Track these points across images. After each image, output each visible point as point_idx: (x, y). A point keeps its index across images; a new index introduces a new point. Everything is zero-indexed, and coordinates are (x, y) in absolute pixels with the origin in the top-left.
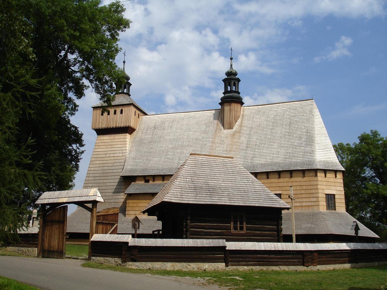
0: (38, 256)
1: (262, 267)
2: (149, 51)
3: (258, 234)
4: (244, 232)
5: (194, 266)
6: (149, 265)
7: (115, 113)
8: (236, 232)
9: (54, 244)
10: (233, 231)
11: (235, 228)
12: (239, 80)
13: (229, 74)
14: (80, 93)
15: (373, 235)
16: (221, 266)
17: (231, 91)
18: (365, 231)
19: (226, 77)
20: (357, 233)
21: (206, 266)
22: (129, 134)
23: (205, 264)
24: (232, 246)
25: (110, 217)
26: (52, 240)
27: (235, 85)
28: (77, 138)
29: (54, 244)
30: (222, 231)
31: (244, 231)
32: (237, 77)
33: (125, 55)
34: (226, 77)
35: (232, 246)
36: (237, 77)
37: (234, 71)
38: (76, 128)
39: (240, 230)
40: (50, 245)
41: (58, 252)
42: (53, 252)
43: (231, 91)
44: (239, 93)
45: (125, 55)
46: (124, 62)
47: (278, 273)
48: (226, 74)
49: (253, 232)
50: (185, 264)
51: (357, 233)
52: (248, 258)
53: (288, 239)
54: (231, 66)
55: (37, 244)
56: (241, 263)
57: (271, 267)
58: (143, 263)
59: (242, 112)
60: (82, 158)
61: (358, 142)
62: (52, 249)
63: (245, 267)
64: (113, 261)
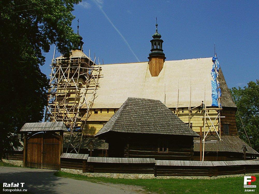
1: (179, 177)
3: (177, 153)
5: (132, 176)
6: (101, 175)
8: (161, 152)
9: (35, 158)
10: (159, 152)
11: (161, 150)
12: (162, 41)
14: (47, 49)
16: (152, 176)
17: (157, 49)
19: (153, 39)
21: (141, 176)
22: (70, 101)
23: (140, 174)
24: (159, 163)
27: (159, 45)
28: (45, 82)
29: (35, 158)
30: (152, 151)
32: (161, 39)
33: (78, 21)
34: (153, 39)
35: (159, 163)
36: (161, 39)
38: (45, 76)
39: (164, 151)
43: (157, 49)
44: (162, 51)
45: (78, 21)
46: (78, 27)
47: (179, 181)
49: (173, 152)
50: (126, 175)
52: (170, 171)
53: (196, 156)
56: (166, 174)
57: (236, 175)
58: (217, 165)
59: (165, 65)
61: (247, 86)
63: (168, 177)
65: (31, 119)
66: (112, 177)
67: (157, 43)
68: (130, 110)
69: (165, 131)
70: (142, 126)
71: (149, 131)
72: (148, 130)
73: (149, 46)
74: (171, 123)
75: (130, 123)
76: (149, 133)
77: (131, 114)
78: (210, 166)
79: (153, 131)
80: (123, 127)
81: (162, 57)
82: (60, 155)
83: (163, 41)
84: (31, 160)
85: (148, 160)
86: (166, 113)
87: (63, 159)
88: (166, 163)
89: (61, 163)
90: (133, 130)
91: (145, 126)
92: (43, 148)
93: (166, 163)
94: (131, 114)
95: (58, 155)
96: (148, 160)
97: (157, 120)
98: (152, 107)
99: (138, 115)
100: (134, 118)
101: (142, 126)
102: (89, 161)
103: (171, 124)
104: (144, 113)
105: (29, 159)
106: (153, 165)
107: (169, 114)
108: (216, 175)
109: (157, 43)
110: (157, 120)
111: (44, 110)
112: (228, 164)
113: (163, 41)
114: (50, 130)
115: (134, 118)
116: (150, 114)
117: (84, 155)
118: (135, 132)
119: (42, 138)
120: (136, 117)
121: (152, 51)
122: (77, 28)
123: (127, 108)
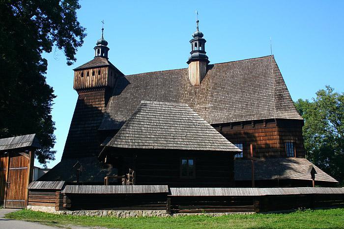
7: (93, 74)
15: (332, 179)
18: (321, 176)
20: (313, 177)
24: (175, 192)
35: (175, 192)
44: (205, 53)
46: (103, 29)
51: (313, 177)
61: (315, 97)
65: (69, 3)
73: (189, 48)
77: (142, 123)
78: (238, 188)
79: (171, 146)
80: (127, 141)
81: (203, 61)
85: (157, 189)
86: (194, 121)
88: (186, 192)
90: (141, 144)
91: (160, 139)
93: (186, 192)
94: (142, 123)
96: (157, 189)
100: (146, 129)
101: (156, 139)
111: (50, 114)
115: (146, 129)
121: (191, 53)
123: (138, 115)
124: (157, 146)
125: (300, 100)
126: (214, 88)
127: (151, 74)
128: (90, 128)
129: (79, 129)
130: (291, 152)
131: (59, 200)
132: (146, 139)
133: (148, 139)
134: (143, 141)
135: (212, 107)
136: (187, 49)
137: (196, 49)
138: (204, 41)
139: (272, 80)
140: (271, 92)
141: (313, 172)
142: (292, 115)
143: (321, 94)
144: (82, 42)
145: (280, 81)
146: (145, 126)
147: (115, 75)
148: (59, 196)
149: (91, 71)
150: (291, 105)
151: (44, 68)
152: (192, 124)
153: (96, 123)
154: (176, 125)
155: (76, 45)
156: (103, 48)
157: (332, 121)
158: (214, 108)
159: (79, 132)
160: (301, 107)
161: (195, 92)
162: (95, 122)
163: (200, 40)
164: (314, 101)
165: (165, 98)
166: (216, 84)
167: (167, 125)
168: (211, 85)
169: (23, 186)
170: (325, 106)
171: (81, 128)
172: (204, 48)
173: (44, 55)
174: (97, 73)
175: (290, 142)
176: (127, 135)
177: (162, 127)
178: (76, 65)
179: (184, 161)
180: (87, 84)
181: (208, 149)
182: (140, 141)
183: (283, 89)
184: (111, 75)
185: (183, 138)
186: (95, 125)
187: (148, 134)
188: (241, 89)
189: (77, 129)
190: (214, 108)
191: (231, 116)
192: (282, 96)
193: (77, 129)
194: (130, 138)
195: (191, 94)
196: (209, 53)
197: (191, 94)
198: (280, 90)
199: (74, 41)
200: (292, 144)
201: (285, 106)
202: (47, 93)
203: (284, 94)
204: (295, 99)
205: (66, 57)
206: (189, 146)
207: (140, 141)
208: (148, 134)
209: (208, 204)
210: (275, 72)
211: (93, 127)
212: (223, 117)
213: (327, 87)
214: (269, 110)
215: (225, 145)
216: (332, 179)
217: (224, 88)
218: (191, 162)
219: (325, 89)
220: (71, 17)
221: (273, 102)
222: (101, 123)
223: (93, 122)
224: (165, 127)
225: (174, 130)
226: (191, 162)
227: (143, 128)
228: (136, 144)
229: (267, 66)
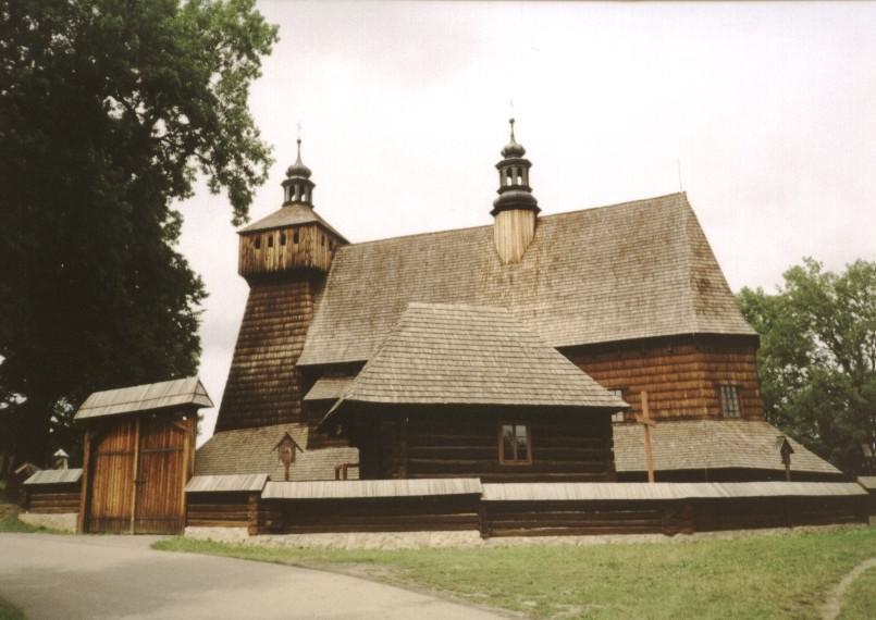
0: (77, 533)
2: (536, 202)
4: (526, 464)
7: (283, 242)
8: (511, 463)
13: (508, 152)
15: (826, 467)
16: (471, 537)
17: (515, 187)
18: (803, 459)
20: (786, 461)
24: (495, 492)
25: (323, 258)
26: (110, 495)
27: (520, 174)
31: (529, 462)
34: (503, 159)
35: (495, 492)
36: (524, 157)
37: (518, 147)
40: (104, 507)
41: (119, 519)
42: (112, 519)
44: (529, 190)
46: (299, 142)
48: (502, 154)
51: (786, 461)
54: (512, 136)
55: (78, 505)
60: (203, 311)
61: (783, 283)
62: (108, 514)
64: (234, 534)
66: (341, 546)
67: (514, 170)
68: (412, 339)
69: (517, 396)
70: (446, 383)
71: (466, 395)
72: (462, 395)
74: (539, 371)
75: (408, 377)
76: (465, 401)
79: (480, 398)
82: (183, 484)
83: (678, 200)
84: (101, 511)
86: (523, 344)
87: (193, 497)
89: (187, 509)
91: (454, 383)
92: (138, 465)
95: (180, 478)
97: (495, 364)
98: (478, 328)
99: (435, 352)
101: (446, 383)
102: (266, 495)
103: (535, 376)
104: (454, 347)
105: (97, 505)
106: (473, 500)
107: (531, 345)
108: (687, 530)
109: (514, 170)
110: (495, 364)
112: (729, 493)
113: (678, 200)
114: (159, 406)
115: (424, 361)
116: (471, 347)
117: (255, 478)
118: (423, 401)
119: (137, 435)
120: (429, 357)
121: (500, 192)
122: (296, 144)
124: (451, 398)
125: (745, 291)
126: (553, 268)
127: (410, 240)
128: (278, 362)
129: (254, 364)
130: (731, 408)
131: (256, 513)
132: (425, 383)
133: (430, 383)
134: (421, 389)
135: (549, 310)
136: (489, 186)
137: (509, 182)
138: (528, 164)
139: (683, 248)
140: (683, 274)
141: (786, 452)
142: (732, 324)
143: (794, 275)
144: (265, 174)
145: (702, 250)
146: (422, 356)
147: (330, 244)
148: (256, 505)
149: (277, 236)
150: (729, 303)
151: (173, 232)
152: (518, 349)
153: (292, 350)
154: (486, 354)
155: (253, 182)
156: (299, 183)
157: (824, 338)
158: (553, 312)
159: (252, 371)
160: (752, 305)
161: (511, 278)
162: (290, 347)
163: (514, 162)
164: (780, 291)
165: (444, 294)
166: (556, 259)
167: (468, 353)
168: (546, 261)
169: (172, 487)
170: (800, 305)
171: (257, 360)
172: (526, 179)
173: (174, 204)
174: (292, 239)
175: (731, 386)
176: (387, 376)
177: (458, 357)
178: (244, 227)
179: (507, 428)
180: (270, 264)
181: (557, 403)
182: (414, 388)
183: (709, 267)
184: (323, 244)
185: (502, 380)
186: (289, 354)
187: (428, 372)
188: (614, 267)
189: (248, 364)
190: (553, 312)
191: (592, 330)
192: (707, 282)
193: (248, 364)
194: (392, 382)
195: (501, 281)
196: (538, 193)
197: (501, 281)
198: (702, 271)
199: (250, 174)
200: (734, 390)
201: (714, 306)
202: (184, 284)
203: (712, 278)
204: (736, 289)
205: (232, 209)
206: (517, 396)
207: (414, 388)
208: (428, 372)
209: (630, 517)
210: (690, 230)
211: (284, 358)
212: (577, 335)
213: (808, 261)
214: (679, 314)
215: (594, 393)
216: (835, 470)
217: (574, 268)
218: (521, 430)
219: (802, 264)
220: (239, 120)
221: (689, 295)
222: (302, 349)
223: (283, 347)
224: (463, 358)
225: (482, 364)
226: (521, 430)
227: (418, 361)
228: (407, 394)
229: (672, 218)
